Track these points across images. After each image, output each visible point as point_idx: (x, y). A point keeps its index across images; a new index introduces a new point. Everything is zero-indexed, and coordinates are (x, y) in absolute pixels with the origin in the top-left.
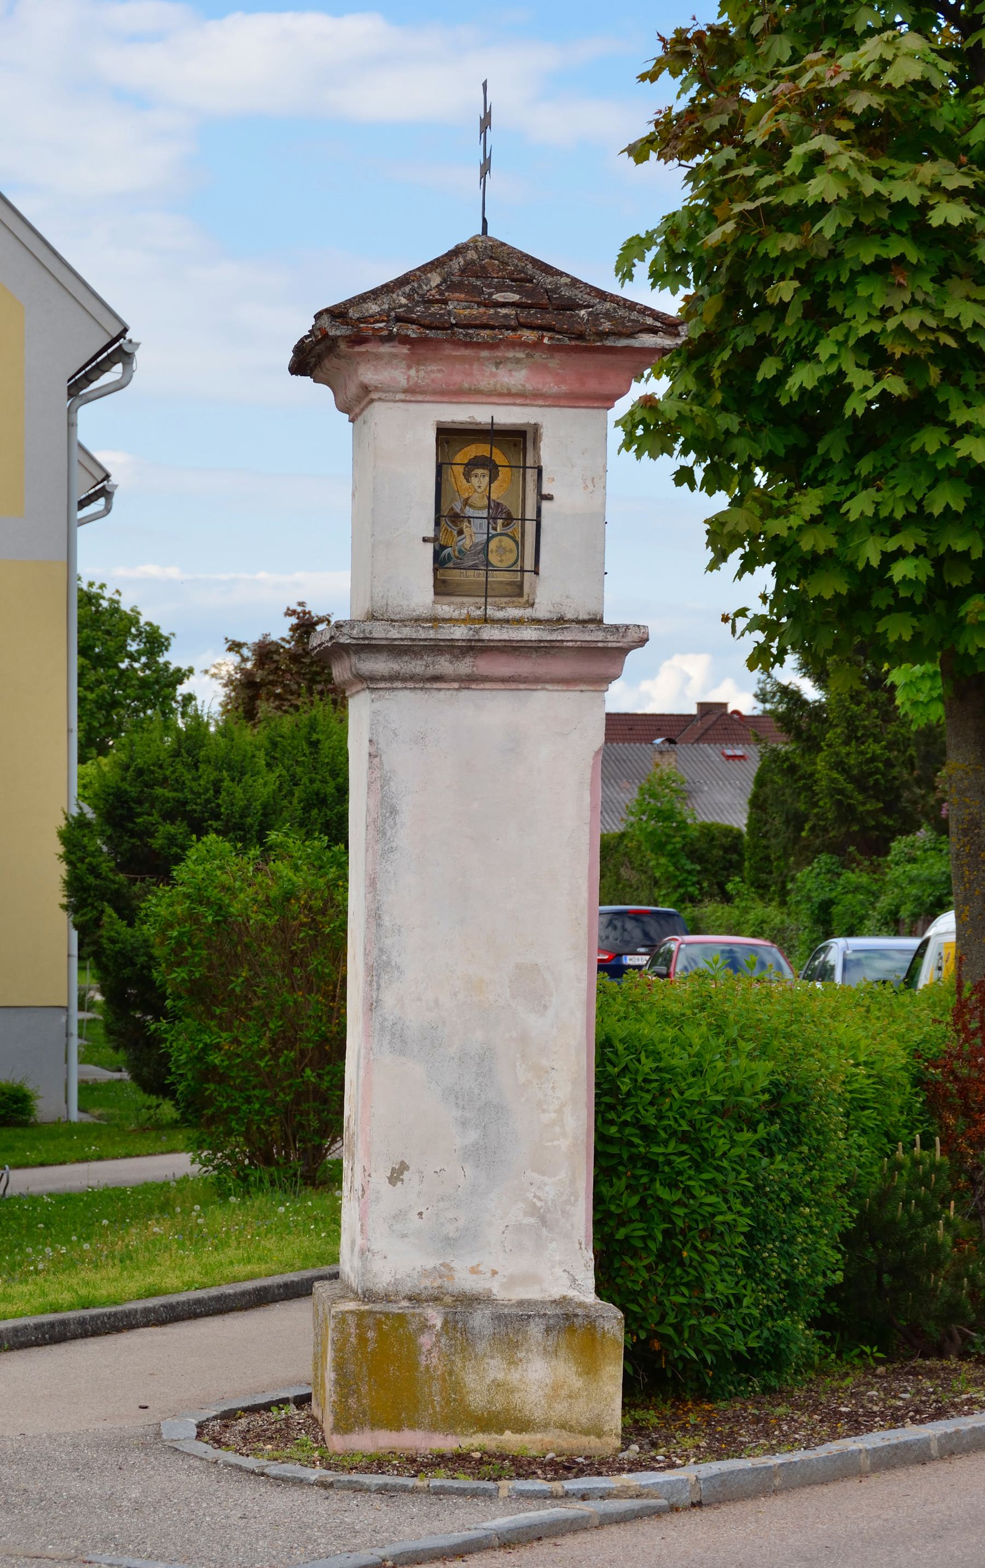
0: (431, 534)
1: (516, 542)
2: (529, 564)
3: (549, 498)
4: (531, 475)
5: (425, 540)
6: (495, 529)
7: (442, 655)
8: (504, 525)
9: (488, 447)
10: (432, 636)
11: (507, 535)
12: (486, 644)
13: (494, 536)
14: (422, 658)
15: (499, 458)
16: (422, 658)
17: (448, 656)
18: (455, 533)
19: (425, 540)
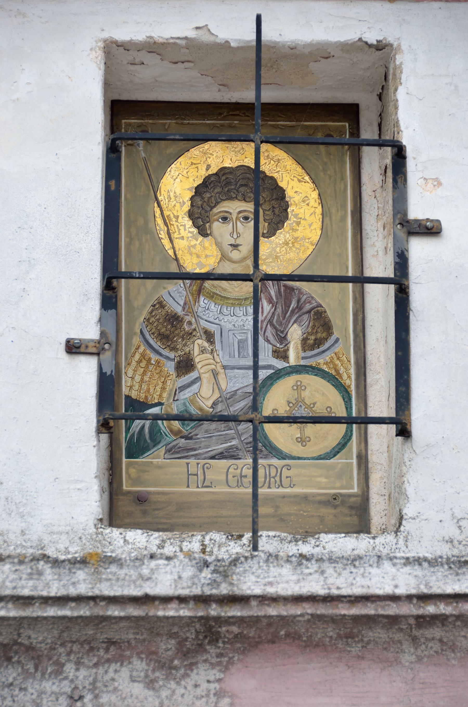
0: (91, 332)
1: (343, 390)
2: (381, 402)
3: (431, 230)
4: (374, 162)
5: (73, 348)
6: (282, 355)
7: (121, 659)
8: (306, 345)
9: (250, 148)
10: (83, 589)
11: (316, 371)
12: (254, 610)
13: (278, 375)
14: (58, 671)
15: (280, 165)
16: (58, 671)
17: (139, 665)
18: (170, 367)
19: (73, 348)
